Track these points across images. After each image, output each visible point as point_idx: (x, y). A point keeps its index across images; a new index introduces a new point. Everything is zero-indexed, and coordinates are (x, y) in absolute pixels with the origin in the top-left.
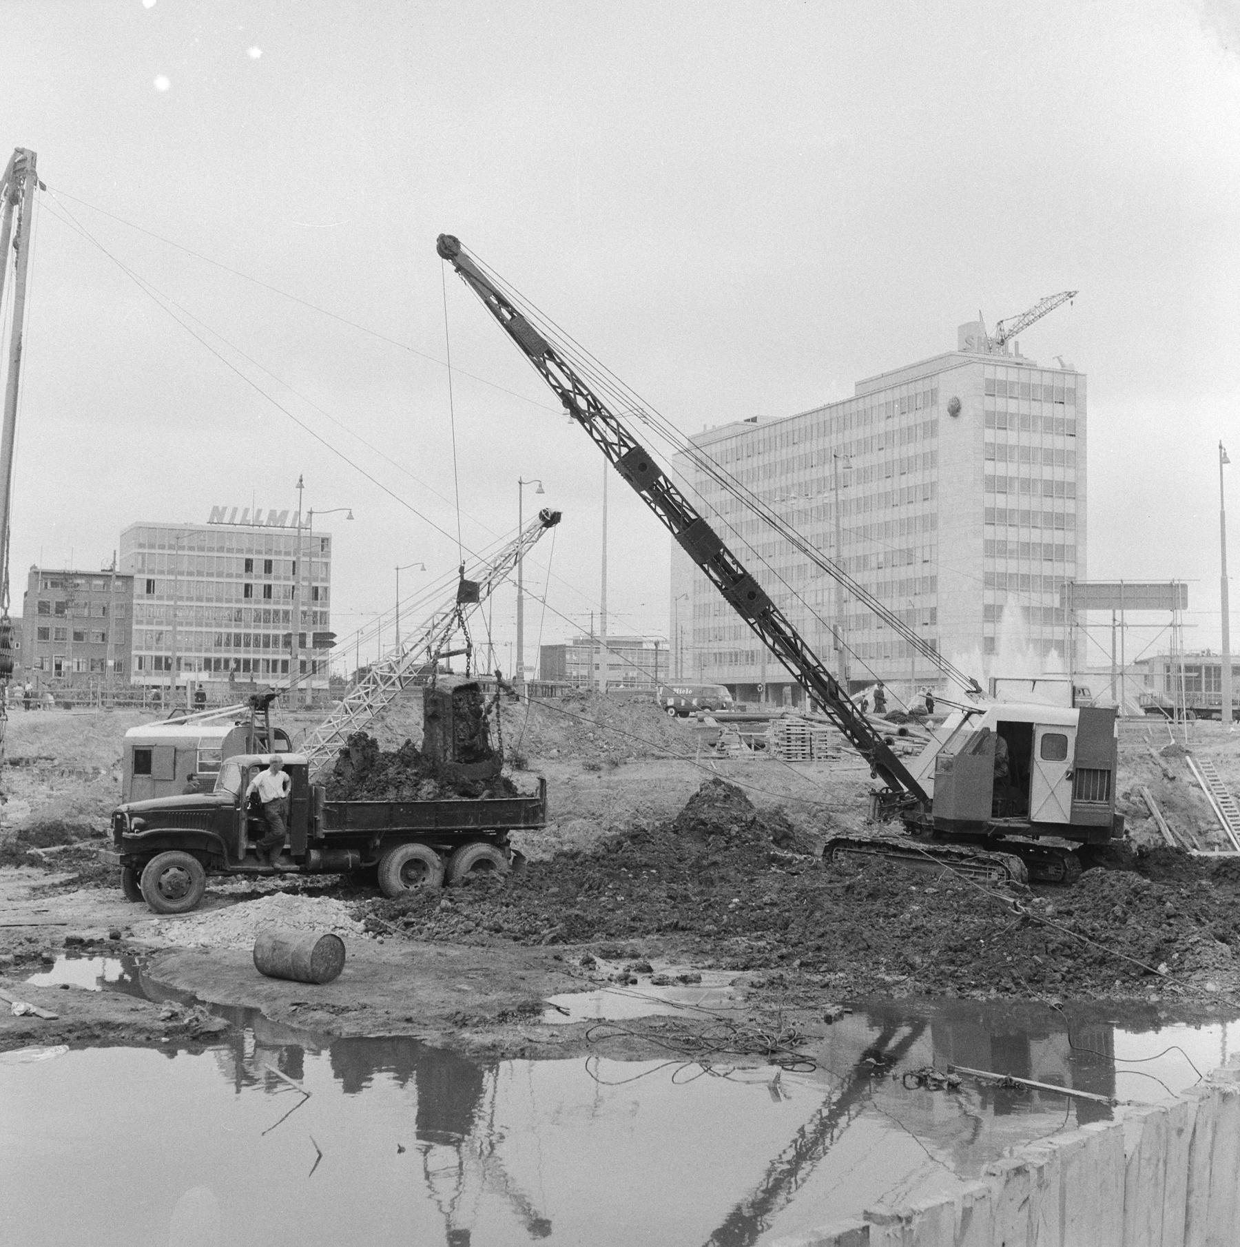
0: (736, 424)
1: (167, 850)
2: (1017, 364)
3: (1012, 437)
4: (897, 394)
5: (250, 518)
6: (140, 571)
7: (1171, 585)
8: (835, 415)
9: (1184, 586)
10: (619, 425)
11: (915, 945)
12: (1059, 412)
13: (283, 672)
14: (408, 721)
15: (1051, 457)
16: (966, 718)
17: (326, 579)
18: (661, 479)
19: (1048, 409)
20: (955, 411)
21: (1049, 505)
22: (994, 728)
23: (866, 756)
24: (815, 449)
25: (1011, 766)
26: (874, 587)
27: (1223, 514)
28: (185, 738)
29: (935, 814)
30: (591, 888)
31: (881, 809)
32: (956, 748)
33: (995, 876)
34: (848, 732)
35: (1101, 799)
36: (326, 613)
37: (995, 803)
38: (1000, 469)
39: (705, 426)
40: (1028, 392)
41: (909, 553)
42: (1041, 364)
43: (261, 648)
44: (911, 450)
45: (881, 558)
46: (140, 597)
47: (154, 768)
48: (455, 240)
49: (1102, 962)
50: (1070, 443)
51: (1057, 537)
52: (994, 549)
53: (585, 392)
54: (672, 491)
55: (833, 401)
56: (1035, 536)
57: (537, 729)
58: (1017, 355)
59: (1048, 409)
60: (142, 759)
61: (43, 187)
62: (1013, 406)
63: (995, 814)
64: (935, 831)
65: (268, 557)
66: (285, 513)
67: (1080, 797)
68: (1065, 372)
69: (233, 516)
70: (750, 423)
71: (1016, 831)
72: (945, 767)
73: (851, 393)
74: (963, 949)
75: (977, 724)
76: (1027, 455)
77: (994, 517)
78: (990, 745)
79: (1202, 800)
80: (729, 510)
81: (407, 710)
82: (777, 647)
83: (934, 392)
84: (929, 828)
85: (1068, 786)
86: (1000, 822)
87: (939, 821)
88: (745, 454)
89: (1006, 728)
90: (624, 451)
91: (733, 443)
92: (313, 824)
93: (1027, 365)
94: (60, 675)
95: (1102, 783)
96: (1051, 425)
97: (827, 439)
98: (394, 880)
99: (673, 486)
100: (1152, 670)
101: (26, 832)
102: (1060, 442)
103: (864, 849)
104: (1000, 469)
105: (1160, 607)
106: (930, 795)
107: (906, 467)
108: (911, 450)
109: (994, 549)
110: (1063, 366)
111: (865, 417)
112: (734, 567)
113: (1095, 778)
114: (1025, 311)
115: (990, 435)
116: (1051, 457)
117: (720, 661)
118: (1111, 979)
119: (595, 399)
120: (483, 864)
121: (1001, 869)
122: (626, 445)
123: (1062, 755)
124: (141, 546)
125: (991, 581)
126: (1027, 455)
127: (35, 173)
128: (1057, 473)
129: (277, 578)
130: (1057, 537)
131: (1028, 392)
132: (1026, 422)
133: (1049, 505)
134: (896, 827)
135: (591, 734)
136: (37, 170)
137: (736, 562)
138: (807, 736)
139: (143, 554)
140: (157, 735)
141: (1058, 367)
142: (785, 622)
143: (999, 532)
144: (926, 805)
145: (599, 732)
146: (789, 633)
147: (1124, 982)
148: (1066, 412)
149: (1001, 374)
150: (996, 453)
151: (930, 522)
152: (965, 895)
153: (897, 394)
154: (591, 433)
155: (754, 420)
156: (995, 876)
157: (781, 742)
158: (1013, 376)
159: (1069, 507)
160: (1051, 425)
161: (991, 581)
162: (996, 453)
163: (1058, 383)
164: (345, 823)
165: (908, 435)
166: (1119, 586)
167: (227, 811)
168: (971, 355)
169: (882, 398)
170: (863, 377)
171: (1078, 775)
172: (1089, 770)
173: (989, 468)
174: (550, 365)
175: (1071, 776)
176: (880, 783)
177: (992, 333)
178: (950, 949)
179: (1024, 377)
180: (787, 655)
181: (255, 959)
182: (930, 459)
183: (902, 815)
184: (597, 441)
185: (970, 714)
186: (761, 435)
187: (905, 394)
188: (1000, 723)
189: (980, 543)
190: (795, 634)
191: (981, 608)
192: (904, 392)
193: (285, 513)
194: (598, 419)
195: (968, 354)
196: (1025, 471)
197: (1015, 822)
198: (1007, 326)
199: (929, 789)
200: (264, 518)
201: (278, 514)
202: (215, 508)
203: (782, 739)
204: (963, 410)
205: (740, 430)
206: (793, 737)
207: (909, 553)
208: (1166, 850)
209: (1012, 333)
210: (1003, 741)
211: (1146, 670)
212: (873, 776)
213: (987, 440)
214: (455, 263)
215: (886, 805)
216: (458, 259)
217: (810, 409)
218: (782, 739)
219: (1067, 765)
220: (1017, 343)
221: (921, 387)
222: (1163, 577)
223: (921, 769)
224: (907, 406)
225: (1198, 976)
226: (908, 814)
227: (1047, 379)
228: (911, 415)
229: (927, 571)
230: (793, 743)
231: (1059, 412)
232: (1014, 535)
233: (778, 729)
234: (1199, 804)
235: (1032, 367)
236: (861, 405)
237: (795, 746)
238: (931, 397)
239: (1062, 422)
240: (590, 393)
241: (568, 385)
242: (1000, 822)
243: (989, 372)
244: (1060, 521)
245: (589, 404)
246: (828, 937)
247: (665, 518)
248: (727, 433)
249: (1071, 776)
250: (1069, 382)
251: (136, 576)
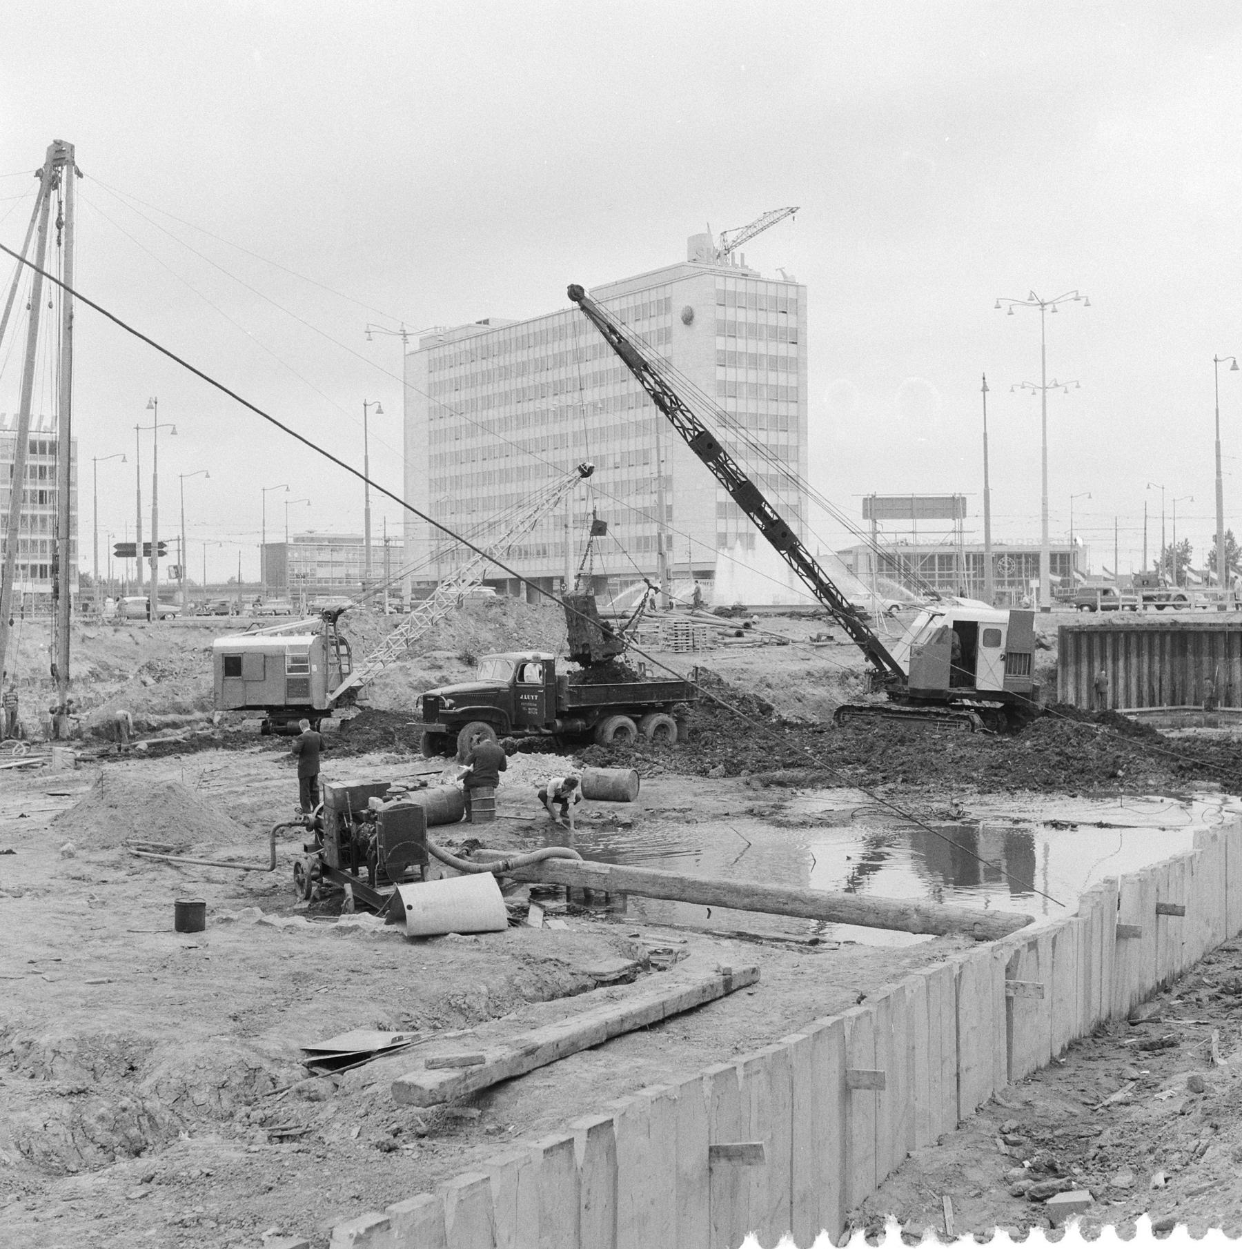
0: (469, 326)
2: (743, 275)
3: (740, 345)
7: (954, 497)
9: (964, 499)
10: (693, 416)
11: (966, 766)
12: (782, 320)
13: (41, 577)
14: (367, 627)
15: (776, 363)
16: (931, 619)
18: (722, 455)
19: (773, 319)
20: (688, 320)
22: (951, 626)
23: (862, 646)
25: (962, 652)
26: (612, 485)
29: (910, 685)
30: (706, 743)
31: (873, 683)
32: (923, 640)
33: (963, 727)
34: (849, 630)
35: (1024, 673)
37: (951, 677)
40: (754, 302)
42: (764, 276)
45: (618, 459)
47: (243, 672)
48: (581, 289)
49: (1082, 771)
53: (670, 394)
54: (729, 462)
57: (472, 631)
58: (743, 266)
59: (773, 319)
60: (232, 665)
61: (80, 175)
62: (741, 316)
63: (951, 685)
64: (911, 698)
67: (1010, 673)
68: (787, 283)
71: (966, 696)
72: (917, 653)
74: (1000, 767)
75: (939, 623)
76: (754, 361)
78: (950, 634)
81: (364, 617)
82: (800, 570)
84: (905, 696)
85: (1002, 665)
86: (955, 691)
87: (914, 690)
88: (479, 355)
89: (957, 625)
90: (696, 433)
91: (466, 345)
92: (558, 700)
93: (754, 276)
95: (1025, 663)
96: (776, 334)
97: (562, 343)
98: (609, 737)
99: (730, 459)
101: (97, 728)
102: (783, 349)
103: (864, 712)
105: (944, 516)
106: (907, 673)
112: (771, 515)
113: (1020, 660)
114: (748, 224)
115: (721, 343)
116: (776, 363)
119: (676, 398)
121: (967, 722)
122: (697, 430)
123: (998, 644)
127: (73, 163)
128: (781, 379)
131: (754, 302)
132: (754, 331)
134: (882, 697)
136: (76, 159)
137: (773, 511)
138: (691, 632)
142: (807, 553)
144: (904, 679)
146: (809, 560)
147: (1099, 782)
148: (789, 321)
149: (730, 285)
150: (727, 360)
154: (672, 421)
155: (486, 322)
156: (963, 727)
157: (669, 637)
158: (741, 286)
159: (792, 410)
160: (776, 334)
162: (727, 360)
163: (782, 292)
164: (581, 700)
166: (911, 499)
171: (1008, 658)
172: (1016, 654)
173: (720, 373)
174: (645, 374)
175: (1004, 658)
176: (870, 665)
177: (718, 245)
178: (993, 767)
179: (751, 288)
180: (807, 576)
183: (886, 688)
184: (677, 427)
185: (934, 616)
186: (494, 338)
188: (955, 622)
190: (813, 561)
191: (714, 505)
192: (639, 300)
194: (678, 412)
195: (698, 265)
197: (964, 691)
198: (731, 237)
199: (906, 669)
203: (671, 635)
204: (696, 317)
206: (679, 633)
208: (1063, 706)
209: (736, 244)
210: (956, 635)
212: (867, 660)
213: (719, 347)
214: (580, 304)
215: (878, 680)
216: (583, 301)
217: (544, 313)
218: (671, 635)
219: (1001, 650)
220: (742, 255)
221: (654, 296)
222: (946, 491)
223: (900, 655)
225: (1141, 776)
226: (890, 687)
227: (772, 290)
230: (680, 637)
231: (782, 320)
233: (666, 626)
235: (757, 279)
238: (665, 306)
239: (785, 330)
240: (674, 395)
241: (658, 389)
242: (955, 691)
243: (720, 283)
244: (782, 424)
245: (672, 401)
247: (724, 481)
248: (458, 336)
249: (1004, 658)
250: (792, 293)
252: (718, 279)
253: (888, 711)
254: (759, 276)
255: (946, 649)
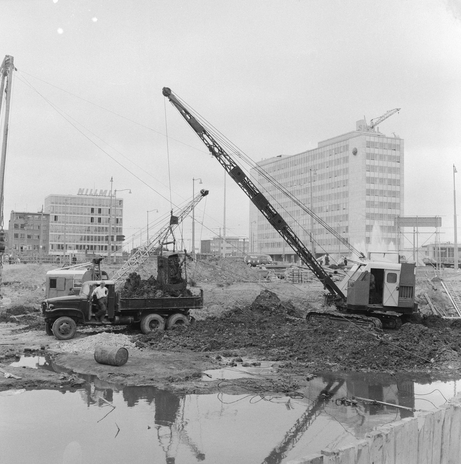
0: (274, 158)
1: (62, 316)
2: (378, 135)
3: (376, 163)
4: (334, 147)
5: (93, 193)
6: (52, 213)
7: (435, 218)
8: (310, 154)
9: (440, 218)
10: (230, 158)
11: (340, 351)
12: (394, 153)
13: (105, 250)
14: (152, 268)
15: (391, 170)
16: (359, 267)
17: (121, 216)
18: (246, 178)
19: (390, 152)
20: (355, 153)
21: (390, 188)
22: (369, 271)
23: (322, 281)
24: (303, 167)
25: (376, 285)
26: (325, 218)
27: (455, 191)
28: (69, 275)
29: (347, 303)
30: (220, 330)
31: (328, 301)
32: (355, 278)
33: (370, 326)
34: (315, 272)
35: (409, 297)
36: (121, 228)
37: (370, 299)
38: (372, 174)
39: (262, 159)
40: (382, 146)
41: (338, 206)
42: (387, 135)
43: (97, 241)
44: (339, 167)
45: (328, 208)
46: (52, 222)
47: (57, 286)
49: (410, 358)
50: (398, 165)
51: (393, 200)
52: (370, 204)
53: (218, 146)
54: (250, 183)
55: (310, 149)
56: (385, 199)
57: (200, 271)
58: (378, 132)
59: (390, 152)
60: (53, 283)
62: (376, 151)
63: (370, 303)
65: (100, 207)
66: (106, 191)
67: (402, 297)
68: (396, 138)
69: (87, 192)
70: (279, 157)
71: (378, 309)
72: (351, 285)
73: (316, 146)
74: (358, 353)
75: (363, 269)
76: (382, 169)
77: (369, 192)
78: (368, 277)
79: (447, 298)
80: (271, 190)
81: (151, 264)
82: (289, 241)
83: (347, 146)
84: (345, 308)
85: (397, 293)
86: (372, 306)
87: (349, 305)
88: (277, 169)
89: (374, 271)
90: (232, 168)
91: (273, 165)
92: (116, 307)
93: (382, 136)
94: (22, 251)
95: (410, 291)
96: (391, 158)
97: (307, 163)
98: (147, 328)
99: (250, 181)
100: (428, 249)
101: (10, 310)
102: (394, 165)
103: (321, 316)
104: (372, 174)
105: (431, 226)
106: (346, 296)
107: (337, 174)
108: (339, 167)
109: (370, 204)
110: (395, 136)
111: (322, 155)
112: (273, 211)
113: (407, 290)
114: (381, 116)
115: (368, 162)
116: (391, 170)
117: (268, 246)
118: (413, 364)
119: (221, 148)
120: (179, 321)
121: (372, 323)
122: (233, 166)
123: (395, 281)
124: (52, 203)
125: (368, 216)
126: (382, 169)
128: (393, 176)
129: (103, 215)
130: (393, 200)
131: (382, 146)
132: (382, 157)
133: (390, 188)
134: (333, 308)
135: (220, 273)
137: (273, 209)
138: (300, 274)
139: (53, 206)
140: (58, 273)
141: (393, 137)
142: (292, 231)
143: (372, 198)
144: (344, 299)
145: (223, 272)
146: (293, 235)
147: (418, 365)
148: (396, 153)
149: (372, 139)
150: (370, 168)
151: (346, 194)
152: (359, 333)
153: (334, 147)
154: (220, 161)
155: (280, 156)
156: (370, 326)
157: (290, 276)
158: (376, 140)
159: (398, 189)
160: (391, 158)
161: (368, 216)
162: (370, 168)
163: (393, 142)
164: (128, 306)
165: (338, 162)
166: (416, 218)
167: (84, 302)
168: (361, 132)
169: (328, 148)
170: (321, 140)
171: (401, 289)
172: (405, 287)
173: (368, 174)
174: (205, 136)
175: (398, 289)
176: (327, 291)
177: (369, 124)
178: (353, 353)
179: (381, 140)
180: (293, 244)
181: (95, 357)
182: (346, 171)
183: (335, 303)
184: (222, 164)
185: (361, 266)
186: (283, 162)
187: (336, 147)
188: (372, 269)
189: (364, 202)
190: (295, 236)
191: (365, 226)
192: (336, 146)
193: (106, 191)
194: (222, 156)
195: (360, 132)
196: (381, 175)
197: (377, 306)
198: (374, 121)
199: (345, 293)
200: (98, 193)
201: (103, 191)
202: (80, 189)
203: (291, 275)
204: (358, 153)
205: (275, 160)
206: (295, 274)
207: (338, 206)
208: (433, 316)
209: (376, 124)
210: (373, 276)
211: (426, 249)
212: (325, 289)
213: (367, 164)
214: (169, 98)
215: (329, 299)
216: (170, 96)
217: (301, 152)
218: (291, 275)
219: (397, 285)
220: (378, 128)
221: (342, 144)
222: (432, 215)
223: (342, 286)
224: (337, 151)
225: (445, 363)
226: (337, 303)
227: (389, 141)
228: (339, 154)
229: (344, 212)
230: (295, 276)
231: (394, 153)
232: (377, 199)
234: (446, 299)
235: (384, 137)
236: (320, 151)
237: (296, 278)
238: (346, 148)
239: (395, 157)
240: (219, 146)
241: (211, 143)
242: (372, 306)
243: (368, 138)
244: (394, 194)
245: (219, 150)
246: (308, 349)
247: (247, 193)
248: (270, 161)
249: (398, 289)
250: (398, 142)
251: (51, 214)
252: (371, 137)
253: (333, 316)
254: (385, 136)
255: (367, 285)
